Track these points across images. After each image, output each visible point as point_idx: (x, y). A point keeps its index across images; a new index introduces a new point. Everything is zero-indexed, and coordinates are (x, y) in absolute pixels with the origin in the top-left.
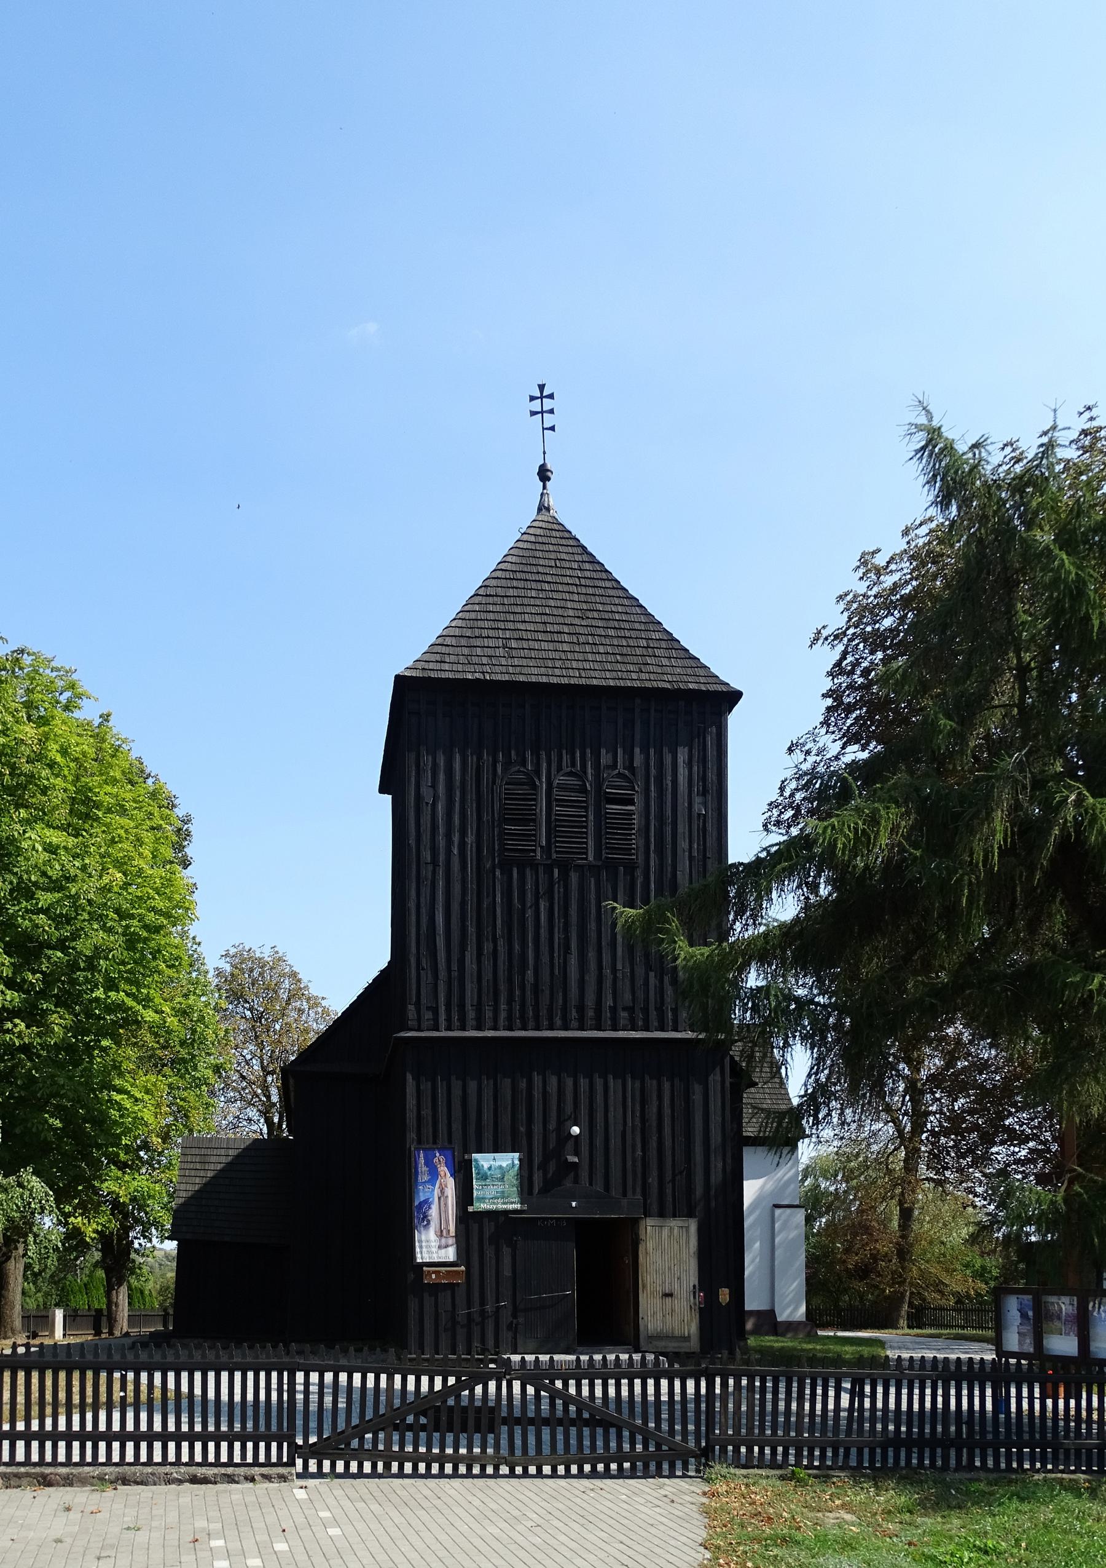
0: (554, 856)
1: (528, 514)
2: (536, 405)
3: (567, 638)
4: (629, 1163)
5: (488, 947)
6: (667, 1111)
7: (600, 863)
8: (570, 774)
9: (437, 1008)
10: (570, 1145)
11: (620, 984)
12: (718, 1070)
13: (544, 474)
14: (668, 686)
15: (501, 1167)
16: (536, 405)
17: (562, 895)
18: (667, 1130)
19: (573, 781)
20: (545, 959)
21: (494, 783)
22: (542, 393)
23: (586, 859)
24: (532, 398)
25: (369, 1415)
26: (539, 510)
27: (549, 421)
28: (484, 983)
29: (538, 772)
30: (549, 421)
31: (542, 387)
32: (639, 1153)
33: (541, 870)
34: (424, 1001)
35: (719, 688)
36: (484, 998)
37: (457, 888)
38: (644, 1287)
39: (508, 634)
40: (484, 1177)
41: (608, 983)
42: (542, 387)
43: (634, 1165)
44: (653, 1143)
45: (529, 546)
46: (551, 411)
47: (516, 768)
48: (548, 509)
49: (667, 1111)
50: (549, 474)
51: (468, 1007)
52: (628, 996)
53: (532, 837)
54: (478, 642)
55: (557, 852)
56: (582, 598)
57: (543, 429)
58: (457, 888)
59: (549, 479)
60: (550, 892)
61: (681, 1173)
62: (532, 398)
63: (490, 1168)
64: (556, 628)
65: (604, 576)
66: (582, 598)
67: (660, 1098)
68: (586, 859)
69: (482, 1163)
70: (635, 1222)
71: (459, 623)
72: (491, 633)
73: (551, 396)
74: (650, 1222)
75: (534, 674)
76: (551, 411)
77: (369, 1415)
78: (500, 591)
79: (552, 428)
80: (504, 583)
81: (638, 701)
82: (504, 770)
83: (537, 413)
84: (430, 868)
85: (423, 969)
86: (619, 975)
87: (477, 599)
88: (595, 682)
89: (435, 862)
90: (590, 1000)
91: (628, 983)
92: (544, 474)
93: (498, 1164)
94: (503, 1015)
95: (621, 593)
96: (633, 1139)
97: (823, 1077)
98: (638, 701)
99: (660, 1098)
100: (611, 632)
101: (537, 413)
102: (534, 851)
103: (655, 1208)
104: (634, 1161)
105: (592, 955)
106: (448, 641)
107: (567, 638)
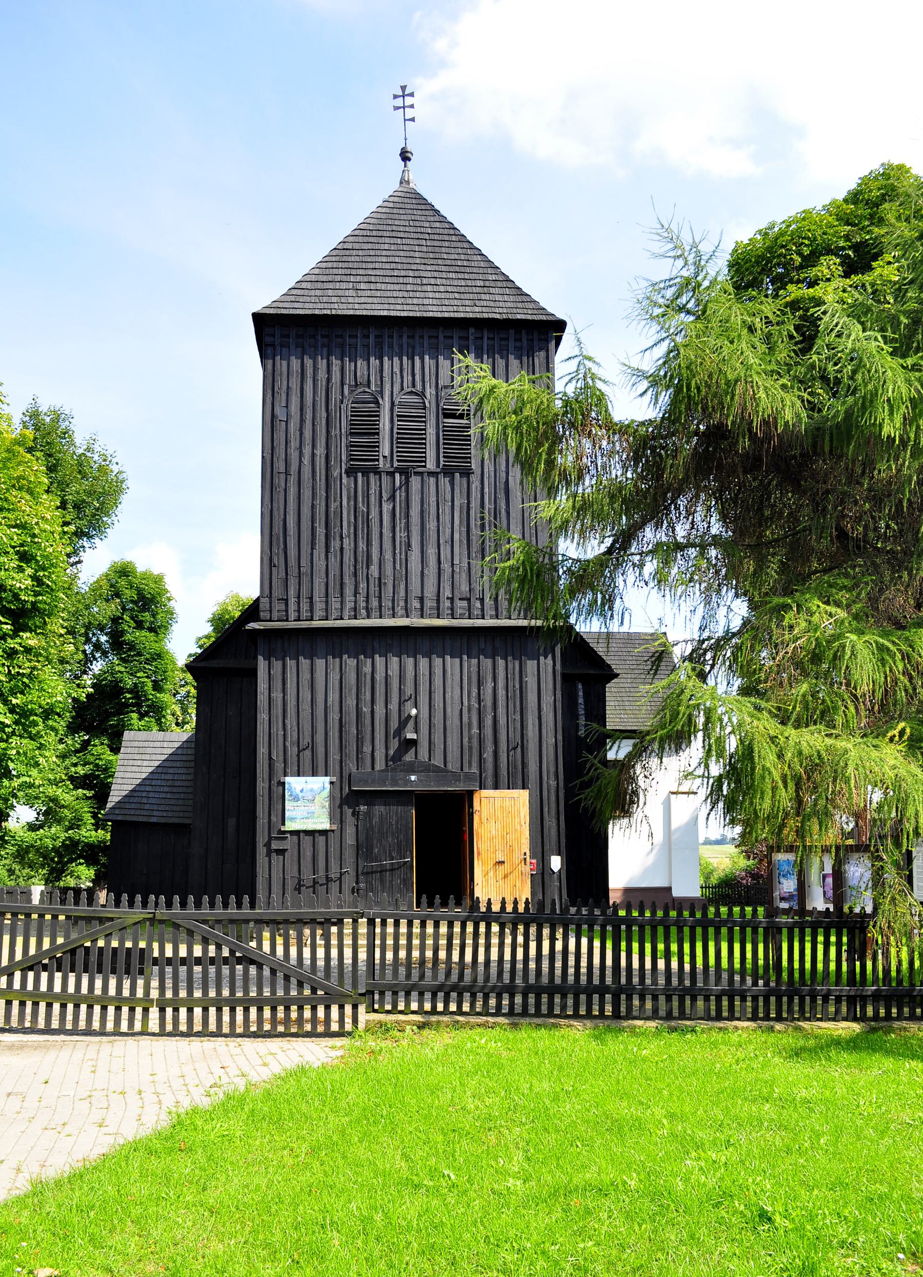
0: (396, 464)
1: (394, 185)
2: (399, 103)
3: (411, 280)
4: (466, 740)
5: (335, 544)
6: (501, 692)
7: (438, 470)
8: (411, 393)
9: (287, 600)
10: (411, 725)
11: (456, 576)
12: (550, 657)
13: (405, 156)
14: (498, 316)
15: (312, 790)
16: (399, 103)
17: (403, 497)
18: (501, 711)
19: (415, 399)
20: (388, 556)
21: (342, 402)
22: (404, 93)
23: (425, 466)
24: (395, 97)
25: (19, 956)
26: (401, 183)
27: (409, 113)
28: (331, 576)
29: (381, 393)
30: (409, 113)
31: (403, 88)
32: (475, 730)
33: (384, 476)
34: (275, 594)
35: (544, 318)
36: (331, 591)
37: (307, 494)
38: (479, 854)
39: (358, 279)
40: (296, 799)
41: (446, 576)
42: (403, 88)
43: (470, 742)
44: (489, 721)
45: (388, 210)
46: (412, 106)
47: (361, 390)
48: (408, 182)
49: (501, 692)
50: (409, 155)
51: (316, 599)
52: (465, 588)
53: (375, 446)
54: (331, 286)
55: (398, 461)
56: (430, 249)
57: (405, 120)
58: (307, 494)
59: (409, 160)
60: (392, 498)
61: (515, 748)
62: (395, 97)
63: (302, 791)
64: (403, 273)
65: (452, 232)
66: (430, 249)
67: (495, 679)
68: (425, 466)
69: (293, 786)
70: (471, 794)
71: (317, 271)
72: (344, 278)
73: (412, 95)
74: (485, 793)
75: (434, 312)
76: (412, 106)
77: (19, 956)
78: (356, 246)
79: (413, 120)
80: (361, 239)
81: (472, 330)
82: (351, 392)
83: (399, 108)
84: (283, 476)
85: (275, 566)
86: (457, 569)
87: (335, 253)
88: (519, 317)
89: (287, 473)
90: (430, 591)
91: (464, 575)
92: (405, 156)
93: (309, 786)
94: (349, 605)
95: (465, 245)
96: (470, 718)
97: (639, 470)
98: (472, 330)
99: (495, 679)
100: (453, 275)
101: (399, 108)
102: (378, 460)
103: (490, 781)
104: (470, 738)
105: (431, 551)
106: (304, 285)
107: (411, 280)
